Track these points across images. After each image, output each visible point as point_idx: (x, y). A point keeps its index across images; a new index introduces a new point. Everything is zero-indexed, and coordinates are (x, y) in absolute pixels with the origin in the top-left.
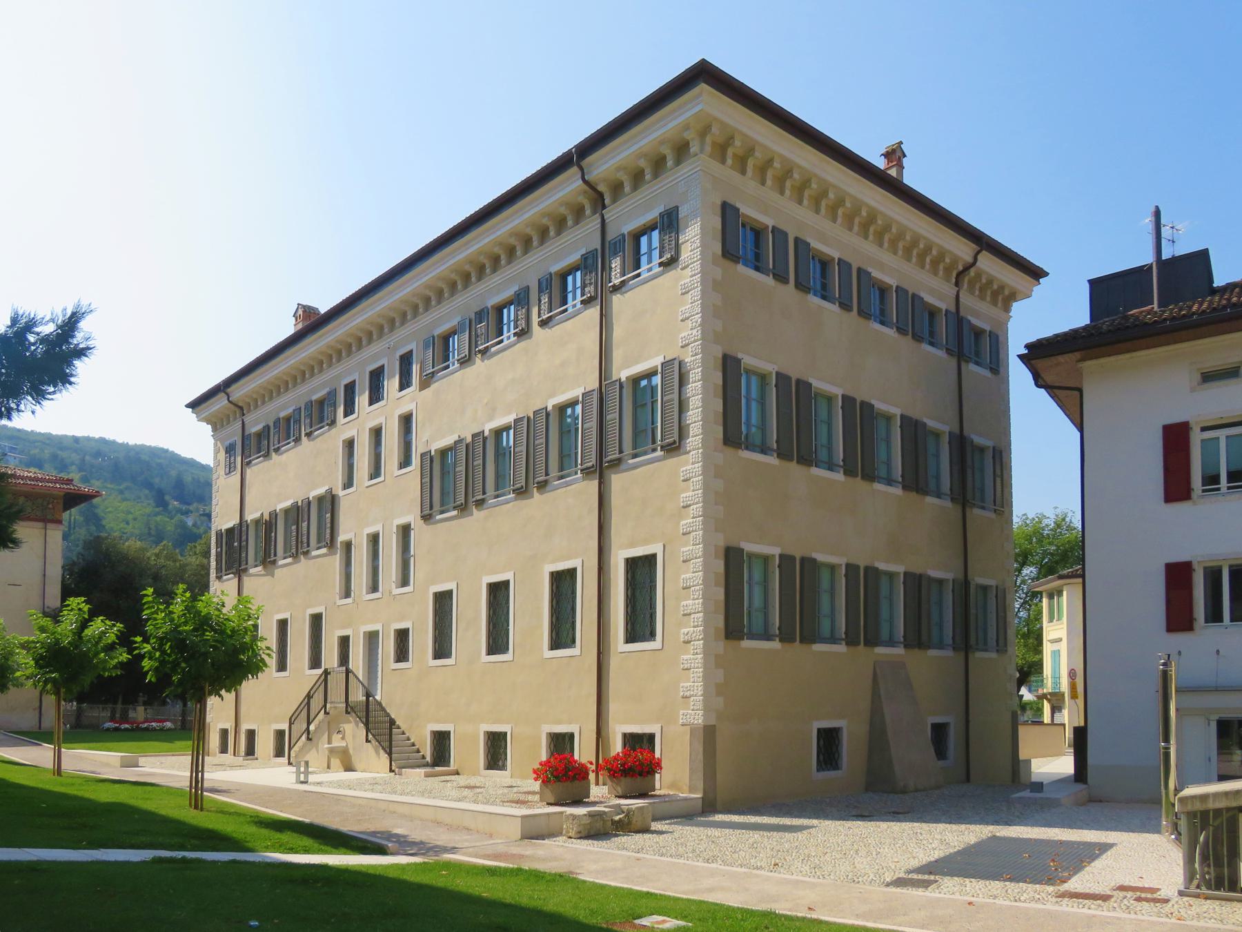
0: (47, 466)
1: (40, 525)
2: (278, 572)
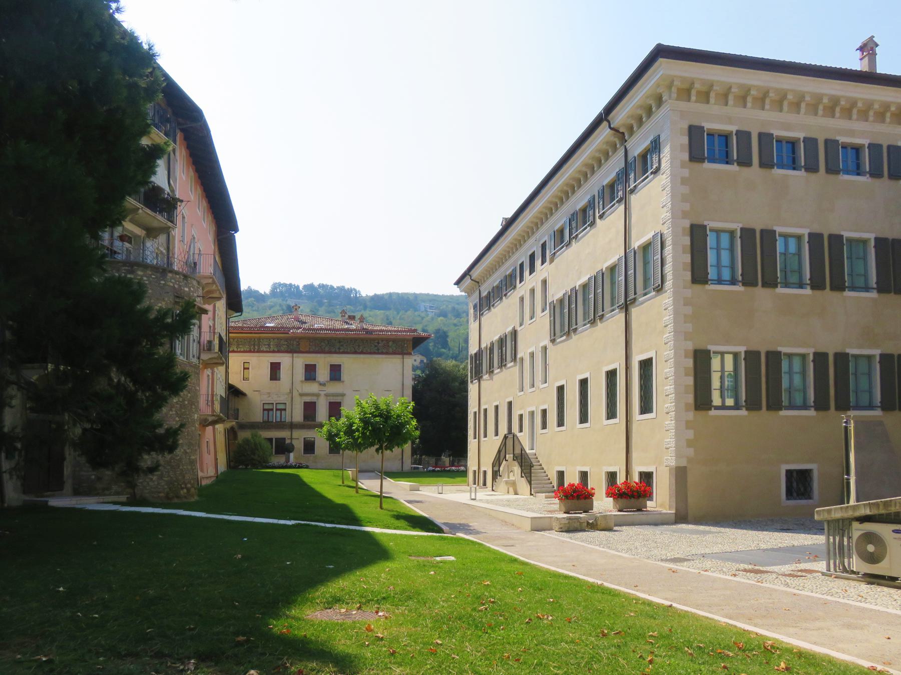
0: (449, 315)
1: (400, 356)
2: (495, 377)
